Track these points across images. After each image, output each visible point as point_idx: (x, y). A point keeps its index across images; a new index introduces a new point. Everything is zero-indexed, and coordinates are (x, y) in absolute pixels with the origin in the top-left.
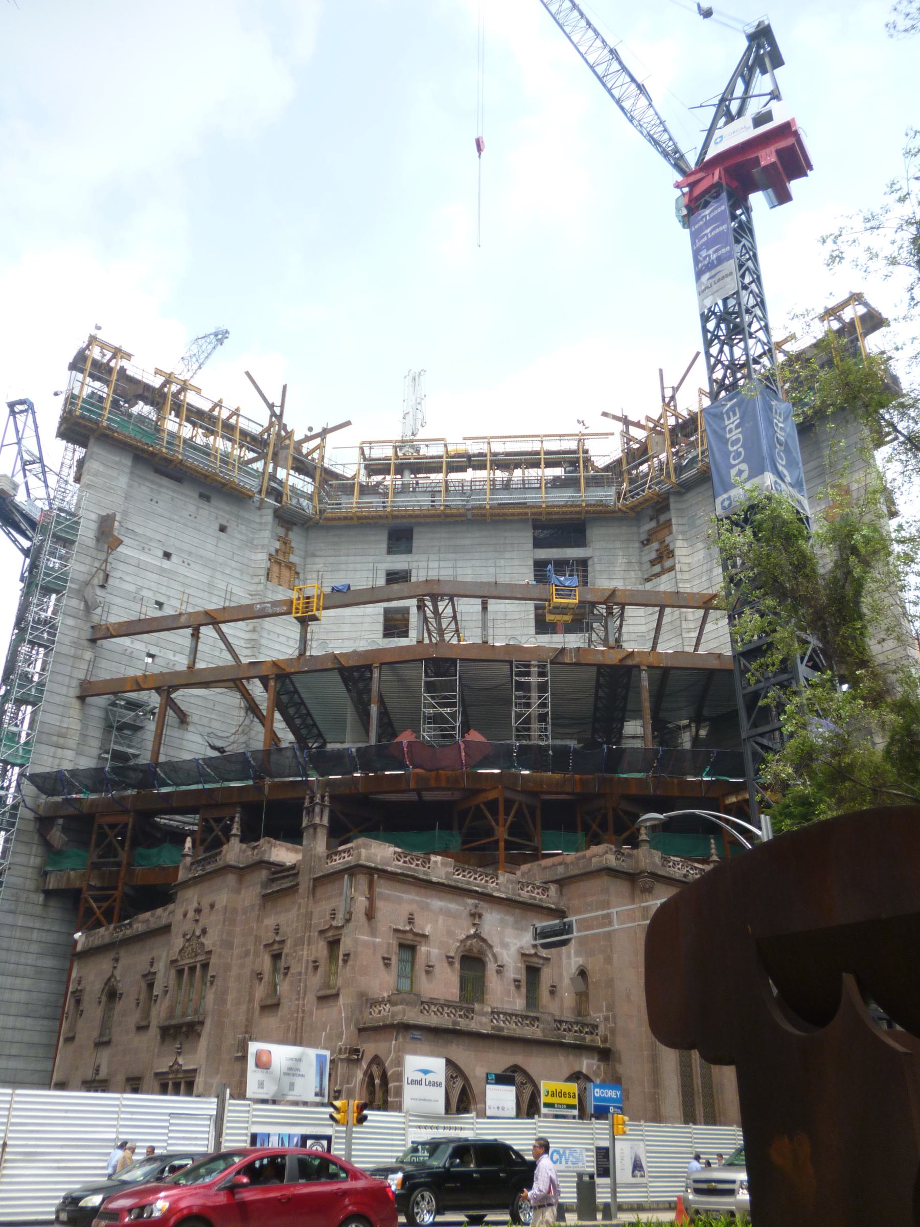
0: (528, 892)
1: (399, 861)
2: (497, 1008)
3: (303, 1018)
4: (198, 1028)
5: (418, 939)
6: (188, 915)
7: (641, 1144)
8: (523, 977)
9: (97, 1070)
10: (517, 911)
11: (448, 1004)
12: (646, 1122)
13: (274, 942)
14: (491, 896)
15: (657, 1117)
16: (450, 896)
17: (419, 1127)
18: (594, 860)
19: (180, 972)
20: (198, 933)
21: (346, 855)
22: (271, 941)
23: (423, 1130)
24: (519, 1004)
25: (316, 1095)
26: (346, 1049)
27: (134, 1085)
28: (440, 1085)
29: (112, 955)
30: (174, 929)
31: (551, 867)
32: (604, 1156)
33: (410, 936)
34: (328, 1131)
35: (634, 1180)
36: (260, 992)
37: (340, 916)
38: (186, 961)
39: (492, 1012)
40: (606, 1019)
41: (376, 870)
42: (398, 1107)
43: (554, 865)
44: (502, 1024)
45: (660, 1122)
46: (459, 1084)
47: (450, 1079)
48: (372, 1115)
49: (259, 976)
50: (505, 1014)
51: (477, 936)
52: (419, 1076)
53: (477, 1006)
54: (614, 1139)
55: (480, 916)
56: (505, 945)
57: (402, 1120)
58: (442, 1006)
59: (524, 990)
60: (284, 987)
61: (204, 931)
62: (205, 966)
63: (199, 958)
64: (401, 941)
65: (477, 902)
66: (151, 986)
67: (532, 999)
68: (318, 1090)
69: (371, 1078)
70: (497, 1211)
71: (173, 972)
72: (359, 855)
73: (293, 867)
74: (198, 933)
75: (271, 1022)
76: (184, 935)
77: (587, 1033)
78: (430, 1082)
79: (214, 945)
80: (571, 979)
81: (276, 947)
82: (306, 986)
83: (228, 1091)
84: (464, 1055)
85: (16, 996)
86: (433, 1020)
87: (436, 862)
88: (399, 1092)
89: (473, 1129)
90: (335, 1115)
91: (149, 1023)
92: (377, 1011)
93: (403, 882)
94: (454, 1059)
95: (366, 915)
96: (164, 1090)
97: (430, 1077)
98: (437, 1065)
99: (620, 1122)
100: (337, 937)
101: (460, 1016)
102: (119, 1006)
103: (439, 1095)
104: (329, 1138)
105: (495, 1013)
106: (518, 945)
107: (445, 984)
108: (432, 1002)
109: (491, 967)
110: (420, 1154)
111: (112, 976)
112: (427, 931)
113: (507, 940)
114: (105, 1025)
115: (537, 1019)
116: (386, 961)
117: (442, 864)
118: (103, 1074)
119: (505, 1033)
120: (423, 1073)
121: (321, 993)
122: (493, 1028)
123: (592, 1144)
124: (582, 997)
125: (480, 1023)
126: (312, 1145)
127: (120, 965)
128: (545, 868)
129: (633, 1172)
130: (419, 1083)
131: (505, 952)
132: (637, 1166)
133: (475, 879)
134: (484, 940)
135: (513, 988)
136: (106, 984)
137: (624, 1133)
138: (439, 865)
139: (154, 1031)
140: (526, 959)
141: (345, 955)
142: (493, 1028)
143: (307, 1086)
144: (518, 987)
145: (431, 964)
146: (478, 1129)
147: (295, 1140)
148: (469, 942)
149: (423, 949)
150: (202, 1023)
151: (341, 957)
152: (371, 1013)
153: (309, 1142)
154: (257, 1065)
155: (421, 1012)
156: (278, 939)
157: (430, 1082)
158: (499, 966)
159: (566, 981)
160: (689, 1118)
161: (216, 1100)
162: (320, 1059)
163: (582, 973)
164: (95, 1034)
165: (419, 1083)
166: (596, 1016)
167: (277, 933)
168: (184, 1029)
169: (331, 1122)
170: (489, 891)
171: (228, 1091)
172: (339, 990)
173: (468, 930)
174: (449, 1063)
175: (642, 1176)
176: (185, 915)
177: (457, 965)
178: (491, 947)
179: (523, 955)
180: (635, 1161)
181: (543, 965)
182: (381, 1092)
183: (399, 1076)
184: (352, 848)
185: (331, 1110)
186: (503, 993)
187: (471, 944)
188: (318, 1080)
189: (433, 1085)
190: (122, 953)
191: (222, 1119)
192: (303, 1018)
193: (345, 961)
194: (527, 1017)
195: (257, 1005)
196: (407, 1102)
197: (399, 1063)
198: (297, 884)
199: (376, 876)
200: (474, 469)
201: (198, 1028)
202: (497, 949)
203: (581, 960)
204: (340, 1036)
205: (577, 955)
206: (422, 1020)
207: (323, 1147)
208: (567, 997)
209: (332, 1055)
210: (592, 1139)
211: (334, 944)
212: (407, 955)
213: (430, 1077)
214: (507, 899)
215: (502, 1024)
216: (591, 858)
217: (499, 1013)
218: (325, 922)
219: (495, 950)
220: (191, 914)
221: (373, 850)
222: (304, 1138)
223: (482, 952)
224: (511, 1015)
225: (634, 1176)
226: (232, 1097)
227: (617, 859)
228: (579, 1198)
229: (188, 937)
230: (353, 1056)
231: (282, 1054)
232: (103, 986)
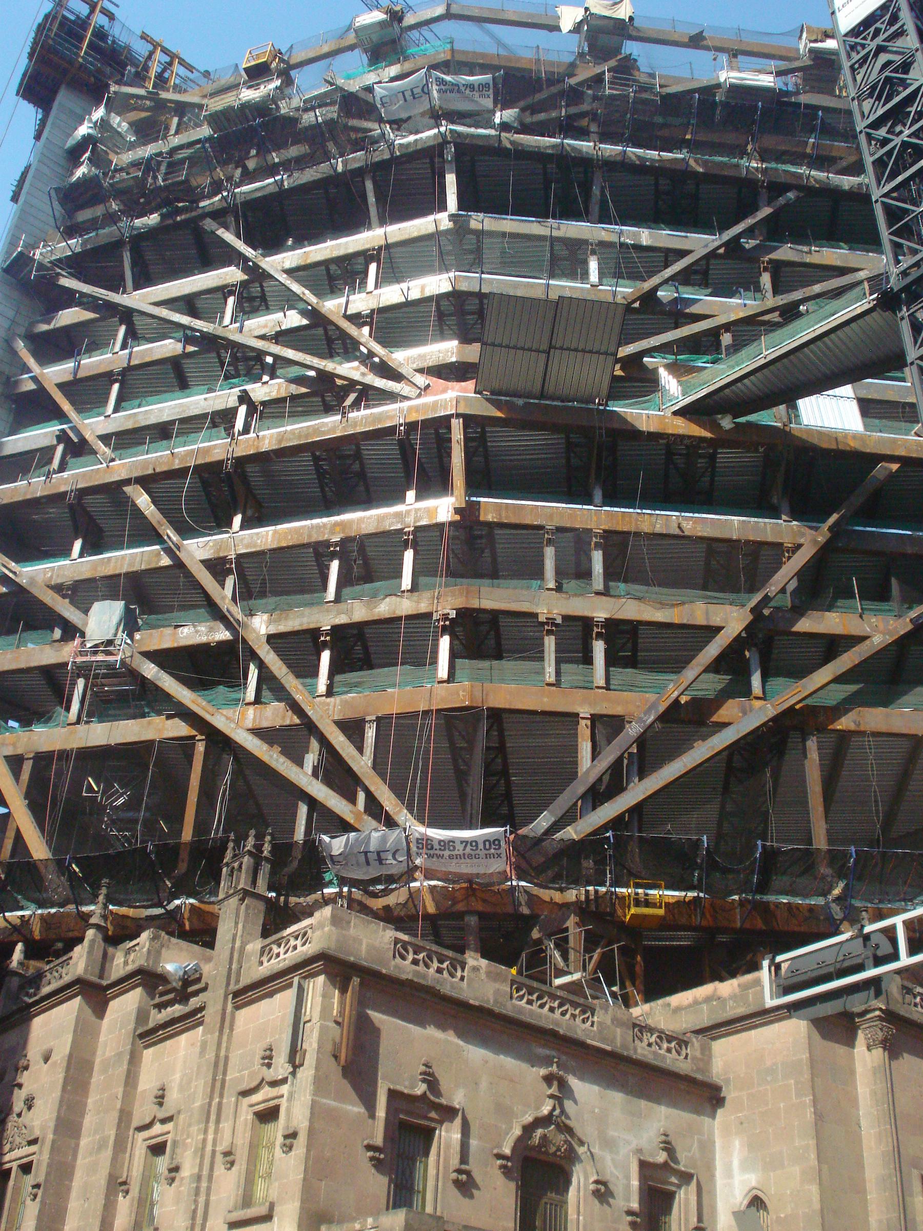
1: (403, 958)
16: (515, 582)
21: (299, 942)
22: (147, 1120)
31: (690, 1006)
43: (696, 1002)
56: (609, 1144)
70: (64, 362)
79: (43, 1128)
80: (735, 1213)
81: (158, 1128)
87: (475, 969)
100: (272, 1103)
106: (633, 1146)
113: (612, 1133)
117: (488, 974)
128: (678, 1010)
131: (608, 1157)
133: (552, 1010)
138: (483, 976)
141: (286, 1137)
151: (280, 1140)
156: (161, 1115)
167: (161, 1104)
172: (272, 1206)
173: (538, 1108)
184: (311, 927)
187: (544, 1137)
200: (535, 615)
205: (744, 1168)
218: (252, 1075)
221: (352, 932)
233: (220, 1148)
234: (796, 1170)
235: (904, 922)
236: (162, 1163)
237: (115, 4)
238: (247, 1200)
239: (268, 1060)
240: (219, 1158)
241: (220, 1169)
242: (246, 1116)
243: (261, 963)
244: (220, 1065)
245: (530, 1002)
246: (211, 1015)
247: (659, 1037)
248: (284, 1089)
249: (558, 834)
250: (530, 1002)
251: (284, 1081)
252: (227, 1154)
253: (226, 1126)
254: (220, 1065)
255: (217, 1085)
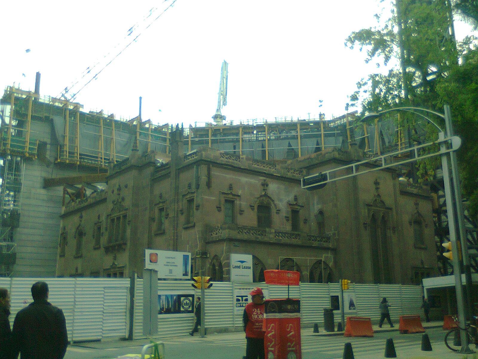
0: (291, 173)
2: (278, 230)
3: (177, 239)
4: (123, 247)
5: (235, 197)
6: (115, 192)
7: (353, 293)
8: (290, 215)
9: (77, 269)
10: (287, 183)
11: (252, 228)
12: (356, 283)
13: (160, 202)
14: (273, 175)
15: (361, 281)
17: (240, 289)
18: (326, 155)
19: (113, 220)
20: (120, 200)
22: (158, 202)
23: (242, 290)
24: (288, 227)
25: (184, 275)
26: (200, 252)
27: (95, 274)
28: (250, 268)
29: (79, 214)
30: (108, 200)
32: (335, 300)
33: (231, 196)
34: (192, 292)
35: (350, 311)
36: (154, 226)
37: (194, 186)
38: (116, 214)
39: (275, 232)
40: (334, 234)
41: (210, 162)
42: (229, 280)
44: (280, 238)
45: (363, 283)
46: (259, 268)
47: (255, 265)
48: (215, 284)
49: (152, 219)
50: (282, 233)
51: (266, 195)
52: (239, 264)
53: (267, 229)
54: (342, 292)
55: (267, 185)
57: (231, 286)
58: (249, 230)
59: (290, 222)
60: (167, 224)
61: (123, 199)
62: (125, 216)
63: (122, 213)
64: (226, 198)
65: (265, 178)
66: (99, 228)
67: (295, 226)
68: (184, 273)
69: (214, 266)
71: (109, 221)
72: (202, 155)
73: (167, 164)
74: (120, 200)
75: (159, 240)
76: (113, 202)
77: (324, 242)
78: (244, 267)
82: (177, 224)
83: (136, 275)
84: (262, 253)
85: (26, 231)
86: (245, 237)
88: (229, 272)
89: (354, 292)
90: (195, 285)
91: (100, 245)
92: (215, 233)
93: (225, 168)
94: (257, 255)
95: (207, 185)
96: (109, 276)
97: (244, 264)
98: (248, 259)
99: (346, 283)
101: (259, 235)
102: (84, 239)
103: (250, 272)
104: (193, 296)
105: (277, 233)
107: (250, 218)
108: (244, 228)
109: (274, 210)
110: (241, 302)
111: (80, 225)
112: (240, 193)
114: (79, 247)
115: (299, 235)
116: (219, 208)
118: (80, 271)
119: (283, 242)
120: (241, 263)
121: (186, 226)
122: (276, 240)
123: (329, 295)
124: (321, 225)
125: (271, 237)
126: (184, 300)
127: (83, 220)
129: (350, 307)
130: (239, 267)
132: (352, 305)
134: (269, 197)
135: (285, 221)
136: (77, 228)
137: (348, 289)
139: (102, 250)
140: (292, 206)
141: (196, 206)
142: (276, 240)
143: (179, 272)
144: (288, 220)
145: (242, 210)
146: (356, 292)
147: (175, 297)
148: (262, 198)
149: (237, 202)
150: (125, 244)
151: (195, 208)
152: (212, 235)
153: (182, 298)
154: (151, 261)
155: (239, 233)
156: (161, 201)
157: (244, 267)
158: (278, 210)
159: (312, 217)
160: (377, 281)
161: (129, 279)
162: (186, 258)
163: (321, 213)
164: (74, 253)
165: (239, 267)
166: (329, 233)
168: (116, 248)
169: (194, 288)
170: (272, 173)
171: (136, 275)
174: (254, 257)
175: (354, 309)
176: (113, 192)
177: (256, 210)
178: (273, 201)
179: (290, 204)
180: (350, 301)
181: (300, 209)
182: (219, 273)
183: (228, 265)
185: (193, 282)
186: (280, 222)
188: (184, 267)
189: (246, 268)
190: (84, 214)
191: (134, 288)
192: (177, 239)
193: (197, 209)
194: (293, 234)
195: (153, 234)
196: (233, 276)
197: (228, 258)
198: (170, 173)
199: (211, 166)
201: (123, 247)
202: (276, 202)
203: (320, 206)
204: (196, 246)
206: (239, 237)
207: (189, 300)
208: (314, 225)
209: (192, 255)
210: (329, 292)
211: (191, 201)
212: (229, 206)
213: (244, 264)
214: (282, 177)
215: (280, 238)
216: (325, 155)
217: (279, 233)
219: (275, 202)
220: (116, 192)
222: (179, 296)
223: (269, 204)
224: (285, 233)
225: (350, 309)
226: (138, 277)
227: (339, 154)
228: (325, 320)
229: (115, 203)
230: (204, 254)
231: (163, 255)
232: (76, 230)
233: (180, 209)
234: (331, 204)
235: (415, 158)
236: (163, 214)
237: (96, 75)
238: (188, 222)
239: (190, 186)
240: (179, 212)
241: (179, 215)
242: (185, 201)
243: (185, 161)
244: (177, 188)
245: (264, 167)
246: (173, 175)
247: (294, 171)
248: (195, 195)
249: (464, 262)
250: (264, 167)
251: (195, 192)
252: (181, 211)
253: (180, 204)
254: (177, 188)
255: (177, 194)
